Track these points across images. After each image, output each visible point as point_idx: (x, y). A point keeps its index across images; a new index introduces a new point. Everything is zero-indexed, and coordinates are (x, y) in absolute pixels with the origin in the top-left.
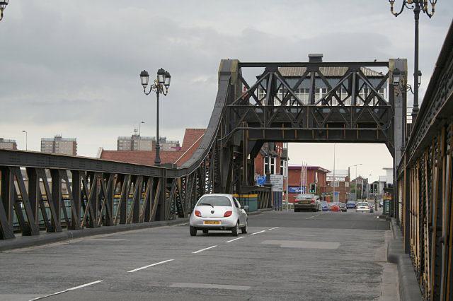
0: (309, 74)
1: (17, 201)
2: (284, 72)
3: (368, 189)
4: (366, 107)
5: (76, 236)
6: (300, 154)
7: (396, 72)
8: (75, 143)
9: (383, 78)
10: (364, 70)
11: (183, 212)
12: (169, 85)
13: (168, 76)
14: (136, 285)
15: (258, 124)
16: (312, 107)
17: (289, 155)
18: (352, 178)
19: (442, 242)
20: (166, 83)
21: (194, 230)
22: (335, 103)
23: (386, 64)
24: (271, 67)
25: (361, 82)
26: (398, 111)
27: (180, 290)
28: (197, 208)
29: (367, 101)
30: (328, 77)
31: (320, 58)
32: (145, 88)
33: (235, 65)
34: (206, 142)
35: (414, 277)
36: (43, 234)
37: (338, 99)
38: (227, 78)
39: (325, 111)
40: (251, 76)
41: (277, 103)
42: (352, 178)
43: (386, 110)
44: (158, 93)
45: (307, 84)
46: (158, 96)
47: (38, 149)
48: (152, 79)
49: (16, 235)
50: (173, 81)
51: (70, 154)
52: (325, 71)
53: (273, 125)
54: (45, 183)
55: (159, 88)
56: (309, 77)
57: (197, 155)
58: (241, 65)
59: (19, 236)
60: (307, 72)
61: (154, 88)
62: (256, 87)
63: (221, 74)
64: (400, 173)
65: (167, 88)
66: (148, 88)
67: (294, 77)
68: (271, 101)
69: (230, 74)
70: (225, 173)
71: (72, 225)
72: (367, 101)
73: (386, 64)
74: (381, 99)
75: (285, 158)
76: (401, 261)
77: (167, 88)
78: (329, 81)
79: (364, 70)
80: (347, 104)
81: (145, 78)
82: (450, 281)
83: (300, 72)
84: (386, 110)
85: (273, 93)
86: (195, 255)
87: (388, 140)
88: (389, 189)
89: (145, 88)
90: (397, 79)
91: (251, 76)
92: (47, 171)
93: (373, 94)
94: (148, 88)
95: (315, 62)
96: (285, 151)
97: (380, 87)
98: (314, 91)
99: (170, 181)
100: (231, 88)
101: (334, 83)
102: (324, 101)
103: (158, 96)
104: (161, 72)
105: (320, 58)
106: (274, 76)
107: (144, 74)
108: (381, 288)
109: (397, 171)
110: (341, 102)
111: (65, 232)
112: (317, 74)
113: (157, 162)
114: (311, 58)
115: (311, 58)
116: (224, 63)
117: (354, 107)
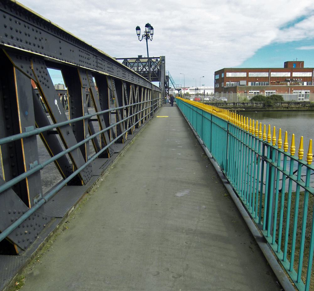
0: (137, 62)
2: (129, 61)
4: (154, 71)
12: (153, 34)
13: (152, 28)
19: (312, 108)
20: (151, 33)
22: (144, 70)
24: (126, 59)
25: (152, 63)
30: (142, 62)
31: (141, 56)
32: (139, 37)
37: (145, 68)
44: (147, 39)
45: (136, 64)
46: (147, 41)
48: (143, 29)
52: (142, 60)
55: (147, 36)
56: (137, 62)
60: (136, 61)
61: (144, 36)
65: (152, 36)
66: (141, 37)
67: (132, 63)
72: (154, 69)
77: (152, 36)
78: (143, 63)
81: (138, 31)
83: (134, 61)
89: (139, 37)
94: (141, 37)
98: (138, 66)
103: (147, 41)
104: (148, 26)
105: (141, 56)
106: (126, 62)
110: (146, 70)
112: (139, 62)
114: (139, 56)
115: (139, 56)
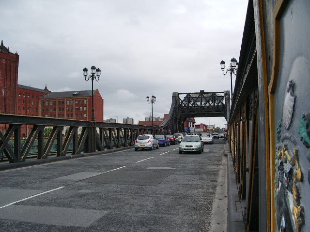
1: (105, 139)
2: (193, 96)
3: (220, 131)
5: (125, 149)
6: (199, 120)
7: (226, 94)
8: (133, 120)
9: (223, 97)
10: (217, 94)
11: (131, 144)
14: (136, 168)
15: (184, 112)
16: (201, 106)
17: (196, 121)
18: (215, 128)
21: (137, 149)
22: (208, 105)
23: (223, 92)
24: (188, 94)
26: (228, 107)
27: (151, 170)
28: (137, 140)
29: (218, 104)
33: (177, 94)
34: (169, 118)
35: (232, 163)
36: (115, 149)
37: (209, 103)
38: (175, 98)
39: (206, 107)
40: (182, 97)
41: (190, 105)
42: (215, 128)
43: (224, 107)
45: (199, 99)
47: (122, 123)
48: (150, 99)
49: (105, 149)
50: (102, 73)
51: (131, 123)
53: (189, 112)
54: (115, 133)
55: (152, 102)
57: (166, 122)
58: (179, 94)
59: (106, 149)
62: (184, 100)
63: (173, 97)
64: (229, 125)
66: (87, 77)
68: (188, 105)
69: (176, 97)
70: (175, 127)
71: (124, 145)
72: (218, 104)
73: (223, 92)
74: (222, 103)
75: (194, 122)
76: (228, 156)
79: (217, 94)
80: (212, 105)
82: (254, 179)
84: (224, 107)
85: (189, 102)
86: (161, 156)
87: (224, 115)
88: (226, 131)
90: (226, 97)
91: (182, 97)
92: (122, 128)
93: (220, 102)
94: (87, 77)
95: (202, 92)
96: (194, 120)
97: (222, 99)
99: (157, 130)
100: (176, 101)
101: (208, 99)
102: (205, 104)
104: (153, 96)
107: (148, 97)
108: (221, 167)
109: (227, 124)
110: (210, 105)
111: (122, 147)
113: (152, 125)
116: (174, 94)
117: (214, 106)
